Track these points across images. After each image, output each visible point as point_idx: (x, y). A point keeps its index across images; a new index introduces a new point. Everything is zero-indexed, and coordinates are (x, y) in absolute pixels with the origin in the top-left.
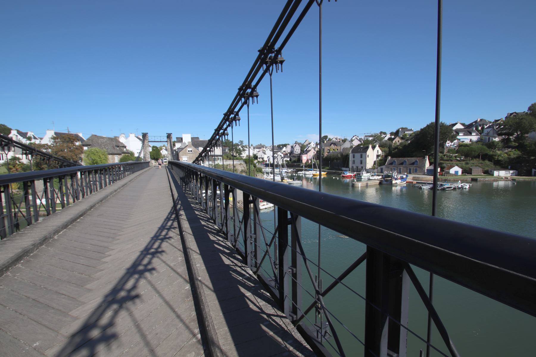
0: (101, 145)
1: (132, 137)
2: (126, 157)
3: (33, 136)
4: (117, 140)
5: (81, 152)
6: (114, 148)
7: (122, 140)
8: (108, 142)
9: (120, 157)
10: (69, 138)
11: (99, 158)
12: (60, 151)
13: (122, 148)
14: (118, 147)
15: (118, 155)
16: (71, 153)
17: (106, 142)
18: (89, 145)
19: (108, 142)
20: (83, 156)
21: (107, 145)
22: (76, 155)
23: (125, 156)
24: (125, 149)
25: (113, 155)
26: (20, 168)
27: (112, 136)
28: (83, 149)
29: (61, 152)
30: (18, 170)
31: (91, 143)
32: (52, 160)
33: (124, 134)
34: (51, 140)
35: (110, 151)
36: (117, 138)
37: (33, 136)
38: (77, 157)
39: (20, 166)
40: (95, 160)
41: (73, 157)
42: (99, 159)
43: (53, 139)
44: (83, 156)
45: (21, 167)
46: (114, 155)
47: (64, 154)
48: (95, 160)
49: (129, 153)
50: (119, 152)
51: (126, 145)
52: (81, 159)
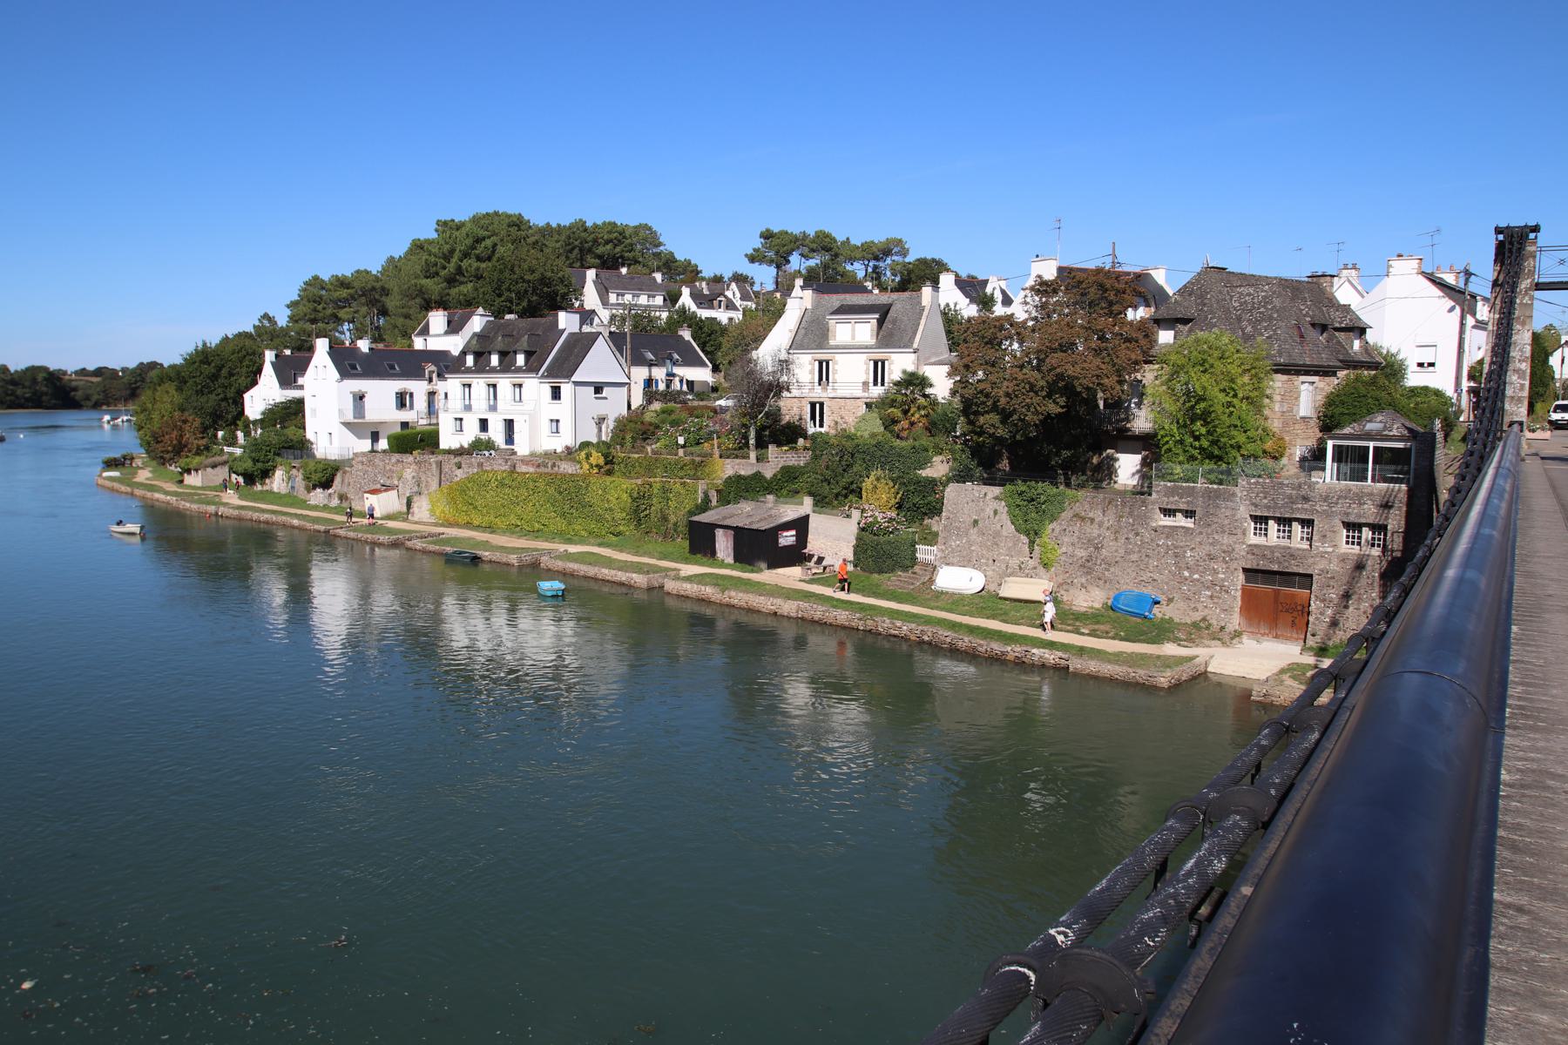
0: (1239, 319)
1: (1405, 277)
2: (1363, 391)
3: (1003, 292)
4: (1322, 291)
5: (1141, 358)
6: (1302, 336)
7: (1344, 293)
8: (1277, 302)
9: (1329, 389)
10: (1102, 287)
11: (1224, 390)
12: (1054, 350)
13: (1341, 336)
14: (1324, 328)
15: (1316, 373)
16: (1098, 361)
17: (1266, 301)
18: (1185, 321)
19: (1277, 302)
20: (1148, 375)
21: (1271, 318)
22: (1119, 373)
23: (1357, 379)
24: (1357, 344)
25: (1294, 377)
26: (924, 420)
27: (1298, 271)
28: (1152, 341)
29: (1060, 355)
30: (248, 465)
31: (1192, 312)
32: (396, 330)
33: (1354, 267)
34: (1028, 300)
35: (1280, 353)
36: (1322, 280)
37: (1003, 292)
38: (1121, 382)
39: (923, 412)
40: (1202, 399)
41: (1106, 381)
42: (1222, 397)
43: (1038, 292)
44: (1148, 375)
45: (926, 416)
46: (1298, 373)
47: (1069, 366)
48: (1202, 399)
49: (1374, 366)
50: (1325, 359)
51: (1366, 317)
52: (1138, 390)
